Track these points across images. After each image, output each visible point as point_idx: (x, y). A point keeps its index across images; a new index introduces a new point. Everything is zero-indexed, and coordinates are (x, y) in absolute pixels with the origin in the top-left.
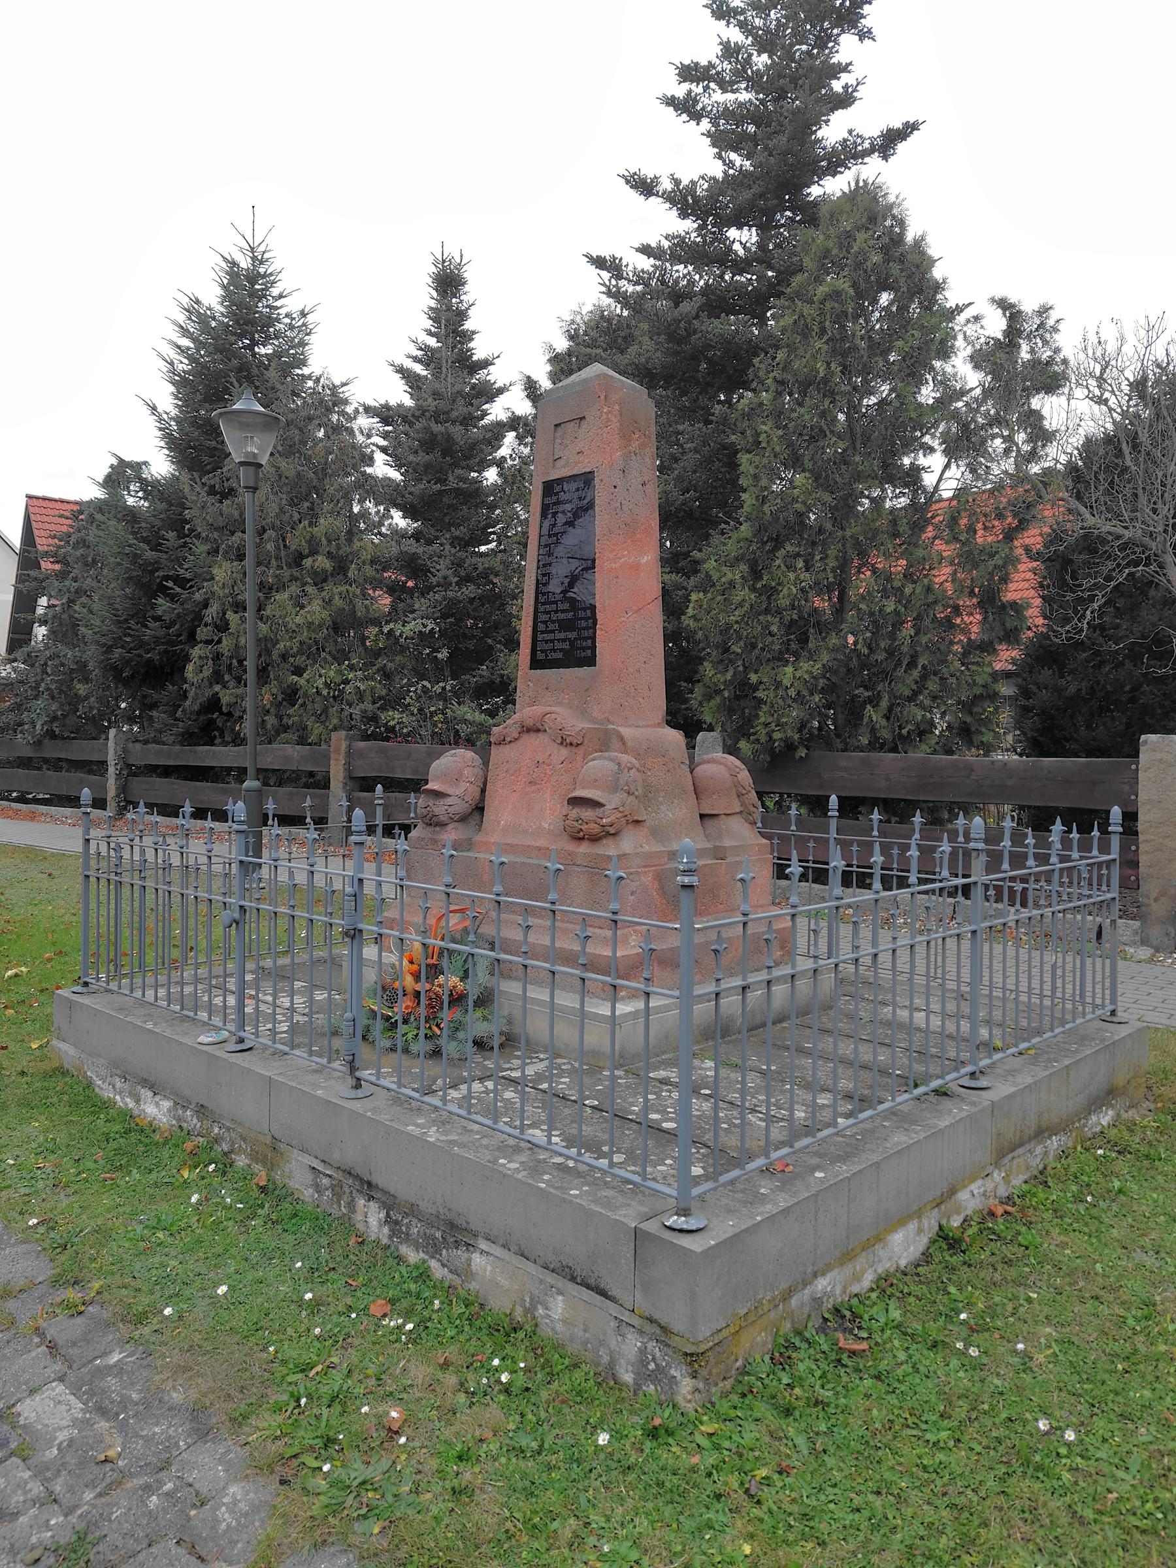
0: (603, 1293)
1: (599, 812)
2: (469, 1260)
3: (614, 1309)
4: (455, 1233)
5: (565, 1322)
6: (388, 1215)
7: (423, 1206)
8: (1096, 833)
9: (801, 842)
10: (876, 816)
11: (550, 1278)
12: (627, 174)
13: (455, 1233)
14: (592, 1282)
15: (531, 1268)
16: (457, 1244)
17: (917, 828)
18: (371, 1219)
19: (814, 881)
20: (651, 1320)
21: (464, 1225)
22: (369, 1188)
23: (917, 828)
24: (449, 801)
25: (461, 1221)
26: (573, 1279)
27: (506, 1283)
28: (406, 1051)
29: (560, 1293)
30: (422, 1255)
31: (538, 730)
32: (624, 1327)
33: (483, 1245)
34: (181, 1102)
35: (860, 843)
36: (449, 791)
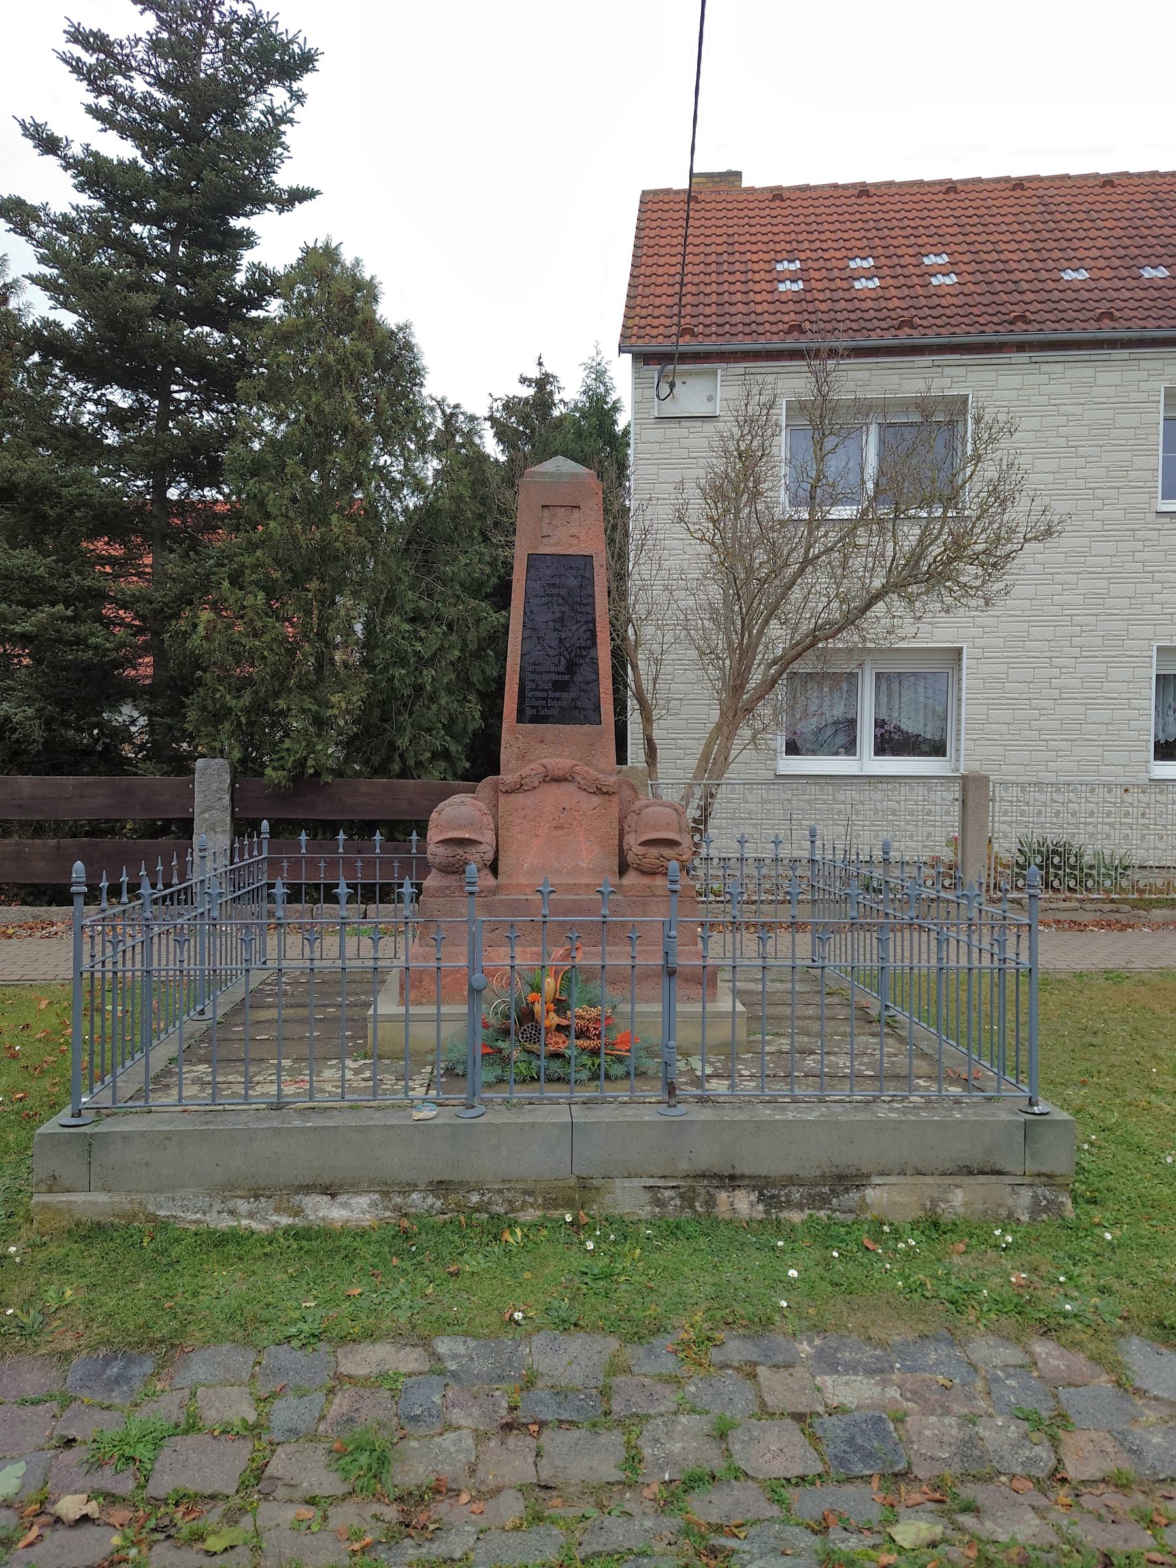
0: (1000, 1173)
1: (677, 850)
2: (863, 1198)
3: (1007, 1179)
4: (848, 1180)
5: (966, 1204)
6: (761, 1194)
7: (802, 1173)
8: (414, 837)
9: (350, 864)
10: (303, 837)
11: (947, 1180)
12: (28, 120)
13: (848, 1180)
14: (988, 1169)
15: (929, 1180)
16: (847, 1190)
17: (303, 844)
18: (744, 1203)
19: (381, 902)
20: (1039, 1175)
21: (855, 1172)
22: (732, 1181)
23: (303, 844)
24: (482, 848)
25: (847, 1172)
26: (970, 1173)
27: (905, 1200)
28: (607, 1077)
29: (958, 1186)
30: (807, 1212)
31: (566, 780)
32: (1017, 1189)
33: (876, 1180)
34: (385, 1189)
35: (401, 860)
36: (480, 839)
